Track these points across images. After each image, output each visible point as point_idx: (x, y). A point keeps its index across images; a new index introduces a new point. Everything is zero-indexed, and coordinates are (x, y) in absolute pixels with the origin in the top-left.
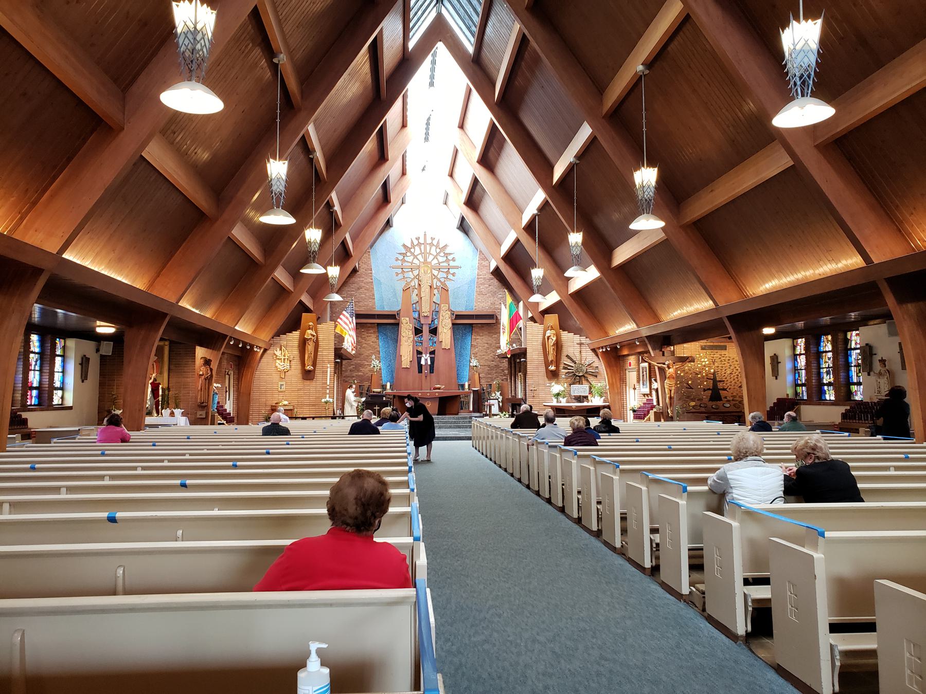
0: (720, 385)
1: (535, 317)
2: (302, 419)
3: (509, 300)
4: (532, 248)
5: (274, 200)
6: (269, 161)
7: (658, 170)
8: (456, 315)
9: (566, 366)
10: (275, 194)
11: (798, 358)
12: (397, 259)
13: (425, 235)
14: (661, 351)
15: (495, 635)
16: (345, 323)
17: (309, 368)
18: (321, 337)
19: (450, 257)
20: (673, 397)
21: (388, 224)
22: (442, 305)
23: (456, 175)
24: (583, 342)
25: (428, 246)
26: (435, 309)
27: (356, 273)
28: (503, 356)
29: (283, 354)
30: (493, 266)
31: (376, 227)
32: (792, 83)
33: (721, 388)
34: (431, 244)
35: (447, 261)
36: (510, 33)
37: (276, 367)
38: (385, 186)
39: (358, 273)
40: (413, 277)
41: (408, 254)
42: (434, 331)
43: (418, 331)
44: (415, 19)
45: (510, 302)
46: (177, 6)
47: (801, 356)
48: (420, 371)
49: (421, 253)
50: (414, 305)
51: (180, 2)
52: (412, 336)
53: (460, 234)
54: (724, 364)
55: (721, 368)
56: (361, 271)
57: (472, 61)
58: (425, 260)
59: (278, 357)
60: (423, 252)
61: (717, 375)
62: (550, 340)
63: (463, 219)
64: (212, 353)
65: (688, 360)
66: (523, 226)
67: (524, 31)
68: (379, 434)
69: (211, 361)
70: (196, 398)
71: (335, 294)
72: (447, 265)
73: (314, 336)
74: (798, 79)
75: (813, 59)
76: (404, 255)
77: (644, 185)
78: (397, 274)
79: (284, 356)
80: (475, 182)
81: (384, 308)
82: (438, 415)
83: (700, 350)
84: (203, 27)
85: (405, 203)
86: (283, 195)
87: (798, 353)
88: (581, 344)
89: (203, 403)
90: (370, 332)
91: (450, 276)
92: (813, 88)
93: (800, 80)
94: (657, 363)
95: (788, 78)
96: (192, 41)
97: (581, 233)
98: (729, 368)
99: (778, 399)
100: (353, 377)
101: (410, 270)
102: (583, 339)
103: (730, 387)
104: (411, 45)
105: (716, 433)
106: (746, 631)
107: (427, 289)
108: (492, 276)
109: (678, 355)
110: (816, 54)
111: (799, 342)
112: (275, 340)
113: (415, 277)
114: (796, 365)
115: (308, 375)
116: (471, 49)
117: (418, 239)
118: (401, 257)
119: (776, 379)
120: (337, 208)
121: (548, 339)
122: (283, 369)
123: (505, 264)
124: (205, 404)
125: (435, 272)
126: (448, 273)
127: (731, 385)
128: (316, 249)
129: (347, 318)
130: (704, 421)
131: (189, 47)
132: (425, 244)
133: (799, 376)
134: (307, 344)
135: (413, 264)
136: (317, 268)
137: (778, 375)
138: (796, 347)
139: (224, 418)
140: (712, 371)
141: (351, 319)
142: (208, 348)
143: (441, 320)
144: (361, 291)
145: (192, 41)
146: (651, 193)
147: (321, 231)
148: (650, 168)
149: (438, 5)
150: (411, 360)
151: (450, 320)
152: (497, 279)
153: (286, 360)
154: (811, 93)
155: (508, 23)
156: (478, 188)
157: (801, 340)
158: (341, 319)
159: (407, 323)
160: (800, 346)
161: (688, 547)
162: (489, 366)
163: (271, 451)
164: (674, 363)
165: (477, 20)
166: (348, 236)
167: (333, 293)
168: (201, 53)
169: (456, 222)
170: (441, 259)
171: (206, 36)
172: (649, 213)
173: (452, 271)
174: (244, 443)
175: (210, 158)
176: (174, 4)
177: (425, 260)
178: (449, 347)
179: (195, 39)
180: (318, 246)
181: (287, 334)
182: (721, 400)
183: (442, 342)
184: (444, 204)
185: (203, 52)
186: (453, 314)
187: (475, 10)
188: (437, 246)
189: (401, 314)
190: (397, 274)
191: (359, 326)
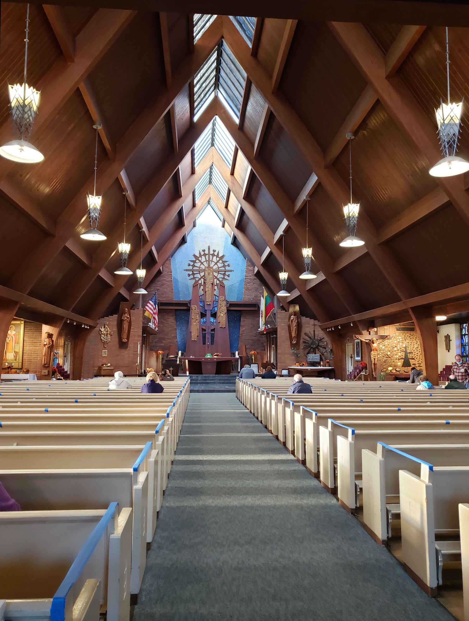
0: (410, 356)
1: (285, 306)
2: (139, 376)
3: (266, 294)
4: (280, 257)
5: (91, 223)
6: (88, 196)
7: (360, 205)
8: (230, 304)
9: (305, 341)
10: (92, 219)
11: (463, 337)
12: (189, 265)
13: (209, 248)
14: (368, 331)
15: (209, 538)
16: (151, 309)
17: (125, 340)
18: (133, 318)
19: (226, 264)
20: (376, 364)
21: (183, 241)
22: (220, 297)
23: (229, 207)
24: (315, 324)
25: (211, 256)
26: (215, 300)
27: (161, 274)
28: (262, 333)
29: (106, 330)
30: (256, 269)
31: (175, 242)
32: (443, 146)
33: (411, 357)
34: (213, 255)
35: (224, 266)
36: (262, 110)
37: (101, 339)
38: (180, 213)
39: (162, 274)
40: (200, 277)
41: (197, 261)
42: (214, 315)
43: (203, 315)
44: (199, 100)
45: (266, 295)
46: (12, 88)
47: (466, 336)
48: (204, 343)
49: (206, 261)
50: (201, 297)
51: (13, 85)
52: (199, 318)
53: (234, 248)
54: (413, 341)
55: (411, 344)
56: (165, 273)
57: (238, 129)
58: (209, 265)
59: (102, 333)
60: (207, 260)
61: (407, 349)
62: (293, 322)
63: (235, 238)
64: (53, 330)
65: (387, 338)
66: (275, 242)
67: (272, 110)
68: (312, 393)
69: (53, 335)
70: (42, 361)
71: (142, 289)
72: (224, 269)
73: (128, 318)
74: (446, 143)
75: (456, 130)
76: (194, 262)
77: (350, 216)
78: (189, 275)
79: (107, 332)
80: (242, 212)
81: (180, 299)
82: (215, 374)
83: (396, 331)
84: (30, 102)
85: (196, 226)
86: (98, 220)
87: (464, 334)
88: (314, 325)
89: (46, 364)
90: (169, 315)
91: (226, 277)
92: (457, 149)
93: (448, 144)
94: (366, 340)
95: (440, 142)
96: (22, 112)
97: (311, 249)
98: (416, 344)
99: (446, 366)
100: (157, 347)
101: (198, 272)
102: (316, 322)
103: (416, 357)
104: (196, 119)
105: (401, 390)
106: (388, 537)
107: (210, 286)
108: (256, 277)
109: (380, 334)
110: (459, 127)
111: (464, 326)
112: (100, 320)
113: (202, 277)
114: (462, 343)
115: (123, 345)
116: (237, 121)
117: (204, 251)
118: (192, 264)
119: (449, 351)
120: (145, 229)
121: (292, 322)
122: (106, 340)
123: (264, 269)
124: (47, 366)
125: (216, 274)
126: (224, 275)
127: (417, 356)
128: (126, 258)
129: (152, 305)
130: (397, 381)
131: (19, 116)
132: (209, 254)
133: (464, 350)
134: (123, 323)
135: (200, 269)
136: (126, 271)
137: (450, 349)
138: (463, 329)
139: (62, 376)
140: (404, 345)
141: (154, 306)
142: (54, 327)
143: (219, 308)
144: (164, 286)
145: (22, 112)
146: (355, 221)
147: (130, 245)
148: (354, 204)
149: (215, 90)
150: (198, 335)
151: (225, 307)
152: (259, 280)
153: (108, 334)
154: (455, 153)
155: (261, 103)
156: (245, 217)
157: (465, 324)
158: (148, 306)
159: (195, 309)
160: (465, 329)
161: (355, 474)
162: (252, 340)
163: (79, 400)
164: (377, 340)
165: (241, 100)
166: (153, 249)
167: (141, 288)
168: (28, 120)
169: (230, 240)
170: (220, 265)
171: (32, 109)
172: (353, 235)
173: (227, 273)
174: (135, 387)
175: (50, 192)
176: (10, 86)
177: (209, 265)
178: (224, 326)
179: (23, 110)
180: (127, 255)
181: (109, 316)
182: (410, 366)
183: (219, 322)
184: (222, 227)
185: (30, 120)
186: (228, 303)
187: (240, 93)
188: (217, 256)
189: (191, 303)
190: (189, 275)
191: (160, 312)
